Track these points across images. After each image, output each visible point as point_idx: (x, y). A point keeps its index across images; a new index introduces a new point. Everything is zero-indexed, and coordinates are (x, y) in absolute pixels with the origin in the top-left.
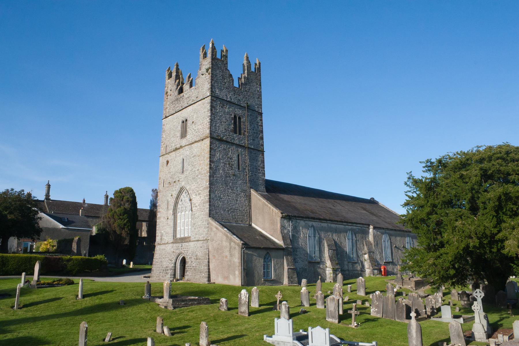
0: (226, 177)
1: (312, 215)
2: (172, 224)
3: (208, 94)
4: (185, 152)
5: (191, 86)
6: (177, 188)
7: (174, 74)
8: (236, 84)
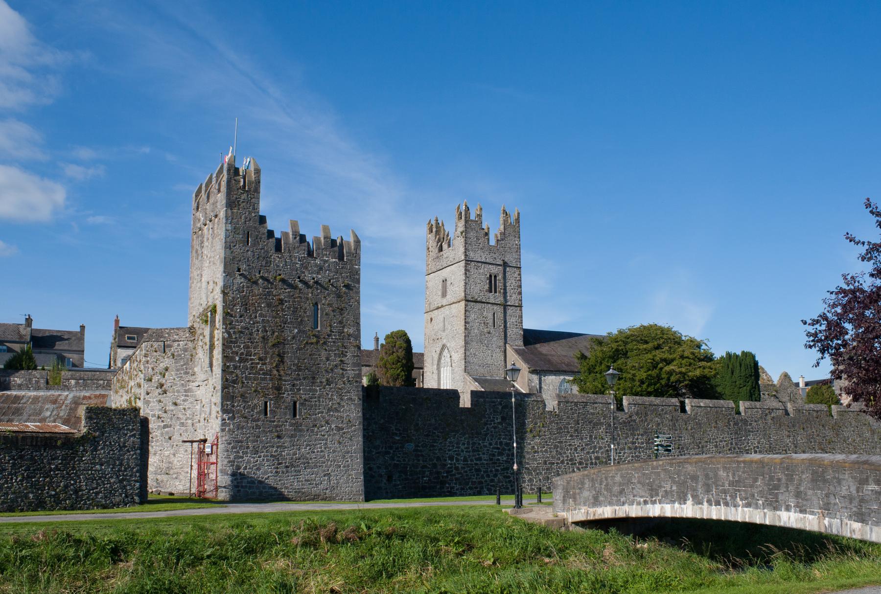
0: (481, 335)
1: (565, 368)
2: (436, 377)
3: (463, 258)
4: (446, 311)
5: (449, 246)
6: (440, 345)
7: (434, 230)
8: (493, 242)
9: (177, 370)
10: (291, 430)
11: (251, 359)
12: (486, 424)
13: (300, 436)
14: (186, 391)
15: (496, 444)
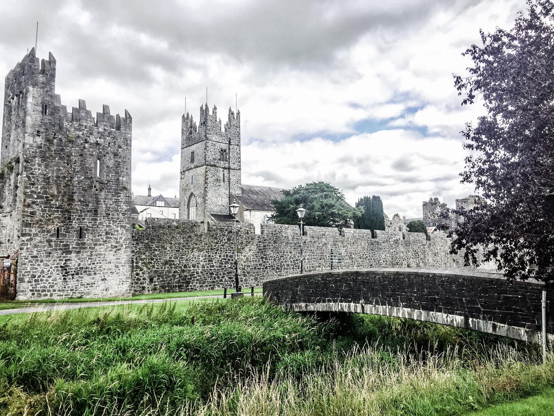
15: (224, 256)
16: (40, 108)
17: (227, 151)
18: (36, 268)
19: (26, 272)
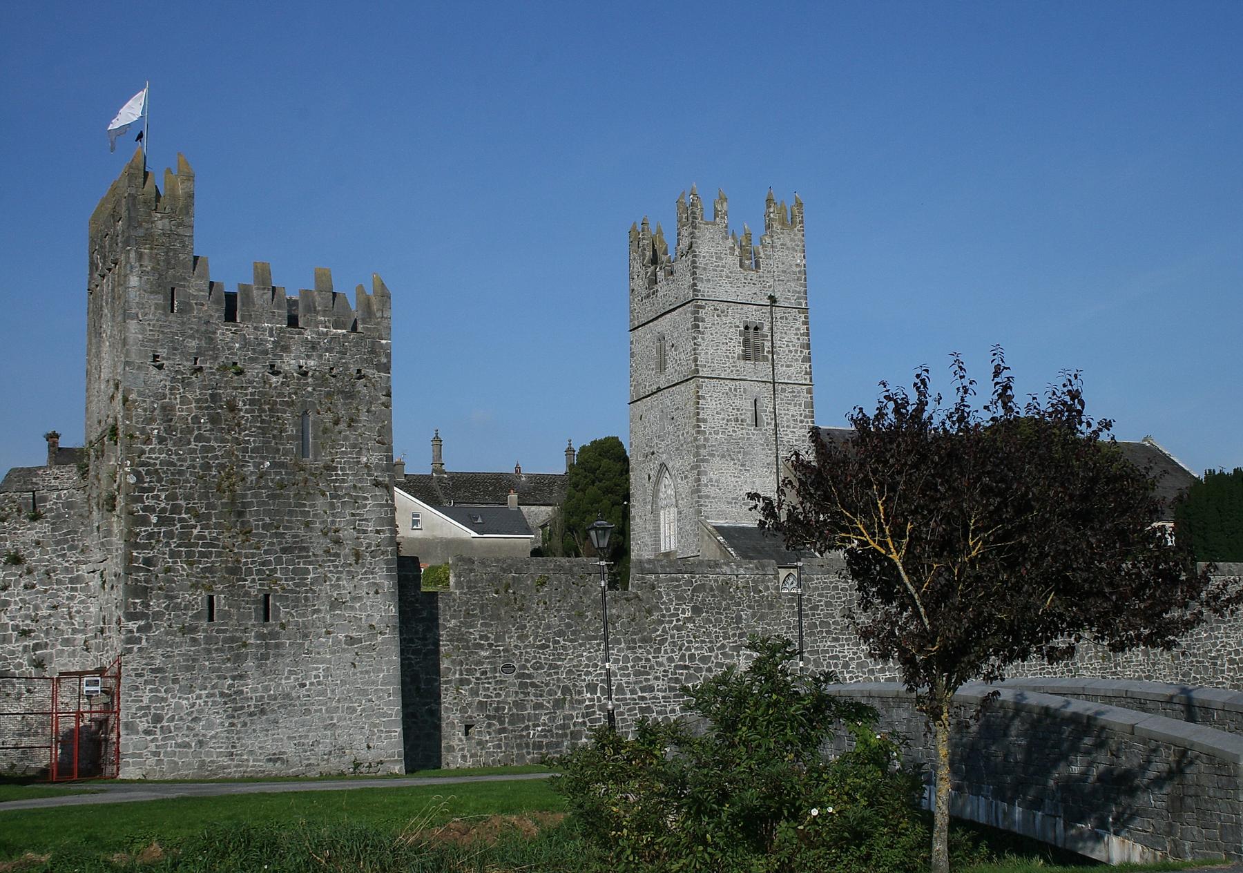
9: (58, 543)
10: (258, 646)
11: (181, 520)
12: (661, 622)
13: (277, 656)
14: (72, 581)
15: (682, 658)
16: (160, 299)
17: (766, 329)
18: (163, 699)
19: (141, 708)
